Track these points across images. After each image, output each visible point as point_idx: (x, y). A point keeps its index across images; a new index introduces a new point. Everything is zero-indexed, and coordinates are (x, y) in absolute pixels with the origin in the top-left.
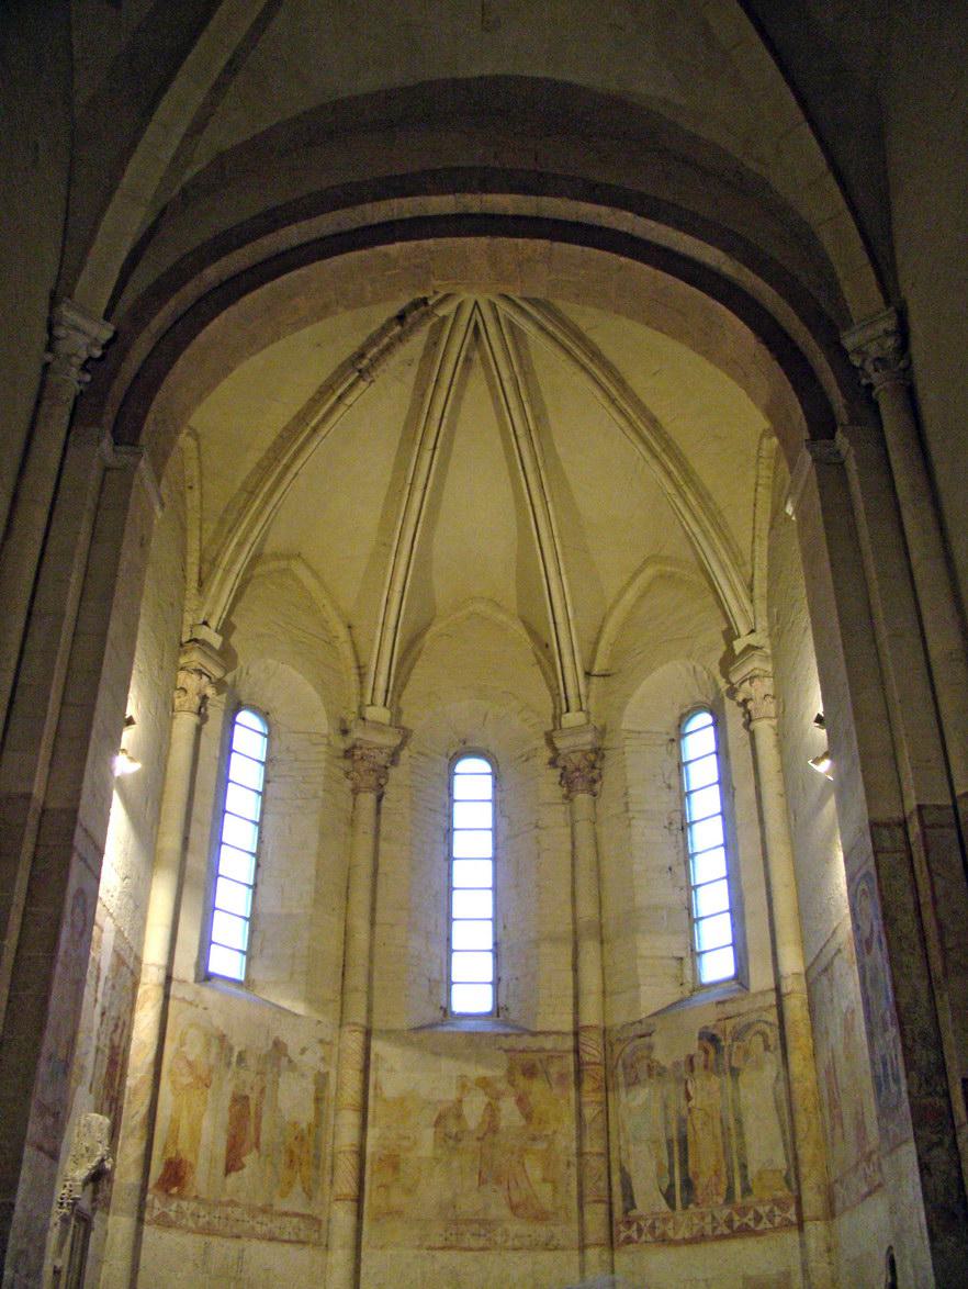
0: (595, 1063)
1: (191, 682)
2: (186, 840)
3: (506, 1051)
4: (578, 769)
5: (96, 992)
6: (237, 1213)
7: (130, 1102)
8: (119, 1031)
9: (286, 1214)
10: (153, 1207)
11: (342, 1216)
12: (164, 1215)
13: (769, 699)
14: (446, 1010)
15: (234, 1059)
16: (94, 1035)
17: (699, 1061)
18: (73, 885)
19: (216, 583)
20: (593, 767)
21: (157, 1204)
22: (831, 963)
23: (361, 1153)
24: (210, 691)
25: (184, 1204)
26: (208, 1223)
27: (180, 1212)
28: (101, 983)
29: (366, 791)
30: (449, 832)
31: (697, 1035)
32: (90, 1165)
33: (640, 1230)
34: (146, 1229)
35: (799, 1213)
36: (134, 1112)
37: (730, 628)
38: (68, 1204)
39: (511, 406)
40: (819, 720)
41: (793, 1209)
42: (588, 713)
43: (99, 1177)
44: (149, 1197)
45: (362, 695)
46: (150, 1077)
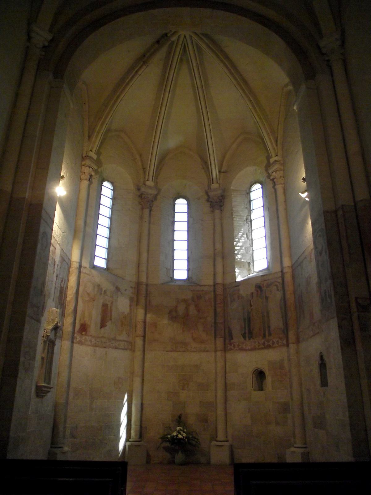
0: (221, 295)
1: (87, 170)
2: (85, 222)
3: (191, 291)
4: (216, 202)
5: (54, 269)
6: (104, 340)
7: (68, 306)
8: (63, 282)
9: (121, 341)
10: (77, 338)
11: (139, 342)
12: (80, 341)
13: (282, 178)
14: (172, 279)
15: (103, 292)
16: (54, 283)
17: (255, 295)
18: (42, 230)
19: (94, 136)
20: (221, 202)
21: (78, 337)
22: (302, 262)
23: (145, 322)
24: (93, 174)
25: (87, 337)
26: (95, 343)
27: (86, 340)
28: (56, 266)
29: (144, 212)
30: (173, 222)
31: (254, 286)
32: (53, 325)
33: (234, 346)
34: (74, 345)
35: (287, 341)
36: (69, 308)
37: (269, 155)
38: (46, 337)
39: (196, 76)
40: (304, 179)
41: (285, 341)
42: (220, 184)
43: (56, 328)
44: (75, 335)
45: (145, 178)
46: (75, 297)
